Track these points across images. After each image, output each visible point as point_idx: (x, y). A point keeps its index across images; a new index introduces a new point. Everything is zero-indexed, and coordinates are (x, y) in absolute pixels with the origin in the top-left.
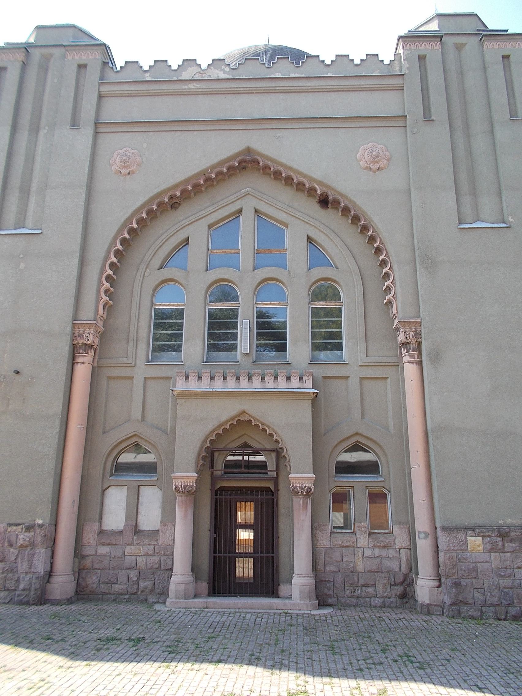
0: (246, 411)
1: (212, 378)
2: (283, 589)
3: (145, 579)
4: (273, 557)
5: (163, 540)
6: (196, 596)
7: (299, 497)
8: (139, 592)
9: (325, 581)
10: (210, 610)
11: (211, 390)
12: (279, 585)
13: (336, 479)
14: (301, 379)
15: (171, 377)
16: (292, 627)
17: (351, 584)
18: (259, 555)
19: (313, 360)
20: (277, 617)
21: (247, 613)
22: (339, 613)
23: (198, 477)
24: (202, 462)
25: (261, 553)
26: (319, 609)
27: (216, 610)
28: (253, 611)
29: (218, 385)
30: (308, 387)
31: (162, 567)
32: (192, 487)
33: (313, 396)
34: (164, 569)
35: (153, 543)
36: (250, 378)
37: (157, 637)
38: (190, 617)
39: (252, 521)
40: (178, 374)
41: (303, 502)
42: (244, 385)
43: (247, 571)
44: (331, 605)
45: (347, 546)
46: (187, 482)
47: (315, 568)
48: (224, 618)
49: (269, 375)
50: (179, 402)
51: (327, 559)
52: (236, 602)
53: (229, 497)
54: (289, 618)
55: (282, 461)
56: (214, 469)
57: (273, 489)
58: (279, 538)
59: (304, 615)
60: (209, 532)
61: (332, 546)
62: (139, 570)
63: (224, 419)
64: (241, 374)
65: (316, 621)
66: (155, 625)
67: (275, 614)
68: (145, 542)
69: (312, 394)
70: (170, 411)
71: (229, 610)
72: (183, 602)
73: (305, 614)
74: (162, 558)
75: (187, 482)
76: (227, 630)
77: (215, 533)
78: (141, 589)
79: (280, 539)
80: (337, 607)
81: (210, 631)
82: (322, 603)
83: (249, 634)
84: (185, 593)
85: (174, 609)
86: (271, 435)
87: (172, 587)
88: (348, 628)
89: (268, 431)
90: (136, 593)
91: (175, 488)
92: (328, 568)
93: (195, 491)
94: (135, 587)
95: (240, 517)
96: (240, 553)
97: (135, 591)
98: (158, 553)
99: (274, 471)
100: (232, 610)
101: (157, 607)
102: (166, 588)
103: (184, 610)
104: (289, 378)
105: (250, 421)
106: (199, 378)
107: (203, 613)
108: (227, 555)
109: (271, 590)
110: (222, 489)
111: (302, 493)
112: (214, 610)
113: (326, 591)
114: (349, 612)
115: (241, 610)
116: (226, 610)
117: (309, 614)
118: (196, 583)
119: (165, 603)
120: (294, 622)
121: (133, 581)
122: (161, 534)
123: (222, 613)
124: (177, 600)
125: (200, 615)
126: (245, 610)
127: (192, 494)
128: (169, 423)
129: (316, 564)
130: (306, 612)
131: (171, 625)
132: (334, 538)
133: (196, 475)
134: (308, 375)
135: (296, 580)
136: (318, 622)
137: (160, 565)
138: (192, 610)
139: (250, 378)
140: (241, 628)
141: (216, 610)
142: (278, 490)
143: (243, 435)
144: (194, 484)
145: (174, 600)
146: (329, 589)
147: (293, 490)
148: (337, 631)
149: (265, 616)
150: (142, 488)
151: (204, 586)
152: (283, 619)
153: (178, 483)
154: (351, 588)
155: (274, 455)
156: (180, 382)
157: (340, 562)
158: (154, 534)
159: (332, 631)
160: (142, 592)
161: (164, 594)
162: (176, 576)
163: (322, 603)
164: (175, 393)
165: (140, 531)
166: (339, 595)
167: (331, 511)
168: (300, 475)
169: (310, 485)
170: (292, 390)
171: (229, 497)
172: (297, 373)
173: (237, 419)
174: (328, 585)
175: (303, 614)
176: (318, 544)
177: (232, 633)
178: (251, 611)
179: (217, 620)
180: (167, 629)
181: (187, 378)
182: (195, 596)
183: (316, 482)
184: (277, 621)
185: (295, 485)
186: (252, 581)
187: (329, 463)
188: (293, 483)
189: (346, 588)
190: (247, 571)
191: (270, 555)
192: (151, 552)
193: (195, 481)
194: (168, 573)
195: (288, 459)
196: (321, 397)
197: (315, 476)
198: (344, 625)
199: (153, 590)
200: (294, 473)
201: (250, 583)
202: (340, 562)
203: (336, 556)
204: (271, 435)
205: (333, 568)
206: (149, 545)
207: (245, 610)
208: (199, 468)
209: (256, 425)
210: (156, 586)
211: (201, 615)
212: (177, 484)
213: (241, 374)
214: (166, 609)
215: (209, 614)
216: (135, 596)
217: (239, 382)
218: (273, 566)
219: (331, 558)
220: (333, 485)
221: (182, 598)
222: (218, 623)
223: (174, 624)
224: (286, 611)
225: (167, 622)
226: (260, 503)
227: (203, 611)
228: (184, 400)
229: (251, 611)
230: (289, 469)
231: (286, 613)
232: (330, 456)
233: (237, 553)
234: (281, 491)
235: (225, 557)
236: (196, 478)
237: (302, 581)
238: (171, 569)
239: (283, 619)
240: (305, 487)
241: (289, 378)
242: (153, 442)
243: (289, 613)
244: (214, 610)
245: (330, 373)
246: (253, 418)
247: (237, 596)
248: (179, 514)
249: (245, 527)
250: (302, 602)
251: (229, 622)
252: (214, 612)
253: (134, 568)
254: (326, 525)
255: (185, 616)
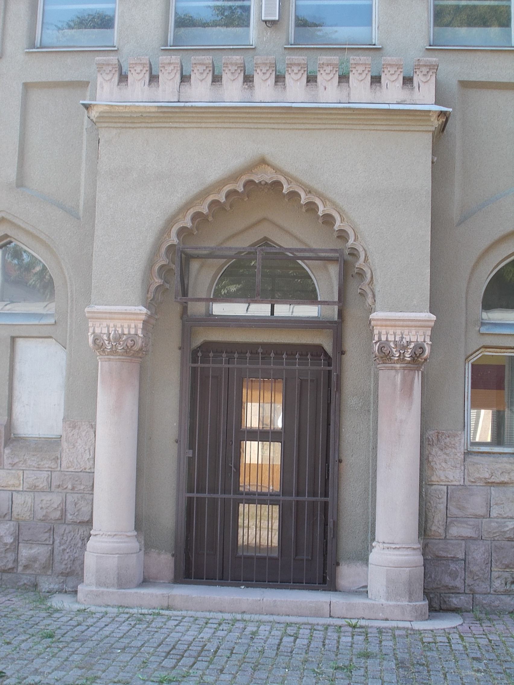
0: (269, 158)
1: (185, 79)
2: (347, 574)
3: (31, 542)
4: (326, 504)
5: (70, 458)
6: (146, 581)
7: (392, 368)
8: (20, 569)
9: (447, 559)
10: (175, 613)
11: (182, 104)
12: (338, 564)
13: (483, 330)
14: (408, 81)
15: (88, 83)
16: (370, 661)
17: (507, 566)
18: (294, 498)
19: (433, 48)
20: (332, 635)
21: (260, 623)
22: (477, 629)
23: (150, 317)
24: (158, 281)
25: (298, 494)
26: (430, 618)
27: (190, 613)
28: (276, 618)
29: (200, 92)
30: (424, 98)
31: (69, 517)
32: (133, 338)
33: (436, 123)
34: (74, 523)
35: (47, 464)
36: (279, 79)
37: (36, 672)
38: (125, 628)
39: (279, 424)
40: (100, 67)
41: (404, 380)
42: (264, 92)
43: (264, 533)
44: (456, 610)
45: (503, 484)
46: (122, 327)
47: (423, 529)
48: (207, 634)
49: (328, 69)
50: (104, 135)
51: (453, 510)
52: (236, 597)
53: (225, 366)
54: (361, 638)
55: (353, 288)
56: (190, 295)
57: (328, 347)
58: (340, 461)
59: (397, 633)
60: (175, 446)
61: (467, 483)
62: (17, 520)
63: (214, 174)
64: (257, 65)
65: (427, 646)
66: (37, 643)
67: (327, 627)
68: (29, 462)
69: (434, 118)
70: (83, 165)
71: (220, 616)
72: (114, 595)
73: (398, 628)
74: (70, 499)
75: (122, 327)
76: (211, 662)
77: (191, 446)
78: (23, 561)
79: (343, 464)
80: (471, 614)
81: (168, 663)
82: (437, 602)
83: (264, 676)
84: (118, 574)
85: (93, 609)
86: (328, 219)
87: (90, 561)
88: (505, 665)
89: (321, 208)
90: (12, 569)
91: (95, 341)
92: (454, 531)
93: (141, 349)
94: (11, 556)
95: (253, 416)
96: (248, 494)
97: (10, 565)
98: (59, 486)
99: (333, 303)
100: (227, 616)
101: (56, 601)
102: (77, 563)
103: (115, 610)
104: (376, 80)
105: (277, 184)
106: (153, 78)
107: (159, 619)
108: (219, 496)
109: (322, 578)
110: (207, 347)
111: (402, 359)
112: (184, 613)
113: (447, 580)
114: (500, 627)
115: (247, 617)
116: (212, 615)
117: (408, 629)
118: (146, 553)
119: (75, 592)
120: (373, 649)
121: (6, 544)
122: (65, 445)
123: (202, 622)
124: (102, 589)
125: (149, 623)
126: (256, 617)
127: (136, 356)
128: (82, 191)
129: (426, 521)
130: (401, 624)
131: (77, 645)
132: (474, 464)
133: (144, 310)
134: (425, 70)
135: (377, 555)
136: (431, 650)
137: (64, 512)
138: (135, 611)
139: (279, 79)
140: (243, 661)
141: (190, 613)
142: (343, 353)
143: (259, 222)
144: (140, 332)
145: (94, 588)
146: (454, 575)
147: (381, 349)
148: (478, 671)
149: (305, 632)
150: (21, 343)
151: (165, 561)
152: (346, 639)
153: (101, 328)
154: (506, 575)
155: (334, 270)
156: (106, 86)
157: (483, 517)
158: (50, 446)
159: (469, 672)
160: (26, 567)
161: (73, 574)
162: (98, 538)
163: (437, 602)
164: (94, 114)
165: (19, 439)
166: (476, 588)
167: (468, 403)
168: (399, 315)
169: (421, 339)
170: (386, 107)
171: (225, 366)
172: (399, 66)
173: (245, 178)
174: (453, 567)
175: (393, 629)
176: (434, 478)
177: (221, 671)
178: (271, 618)
179: (188, 638)
180: (64, 654)
181: (123, 78)
182: (143, 582)
183: (436, 332)
184: (331, 644)
185: (384, 338)
186: (275, 554)
187: (467, 293)
188: (380, 334)
189: (495, 574)
190: (264, 533)
191: (320, 499)
192: (43, 485)
193: (140, 325)
194: (82, 530)
195: (369, 276)
196: (454, 127)
197: (434, 317)
198: (493, 656)
199: (49, 565)
200: (382, 310)
201: (271, 559)
202: (483, 517)
203: (476, 504)
204: (328, 219)
205: (467, 532)
206: (39, 469)
207: (256, 617)
208: (151, 295)
209: (294, 195)
210: (57, 558)
211: (153, 625)
212: (98, 331)
213: (257, 65)
214: (76, 607)
215: (172, 623)
216: (10, 575)
217: (251, 88)
218: (326, 524)
219: (461, 508)
220: (475, 343)
221: (113, 586)
222: (190, 645)
223: (83, 641)
224: (354, 622)
225: (68, 638)
226: (297, 381)
227: (159, 614)
228: (114, 132)
229: (271, 618)
230: (370, 301)
231: (354, 627)
232: (472, 273)
233: (242, 494)
234: (347, 353)
235: (214, 501)
236: (143, 317)
237: (394, 558)
238: (89, 523)
239: (346, 639)
240: (409, 343)
241: (376, 80)
242: (43, 237)
243: (361, 627)
244: (184, 613)
245: (478, 75)
246: (285, 175)
247: (238, 586)
248: (104, 400)
249: (262, 435)
250: (391, 603)
251: (215, 643)
252: (184, 617)
253: (7, 518)
254: (455, 436)
255: (115, 626)
